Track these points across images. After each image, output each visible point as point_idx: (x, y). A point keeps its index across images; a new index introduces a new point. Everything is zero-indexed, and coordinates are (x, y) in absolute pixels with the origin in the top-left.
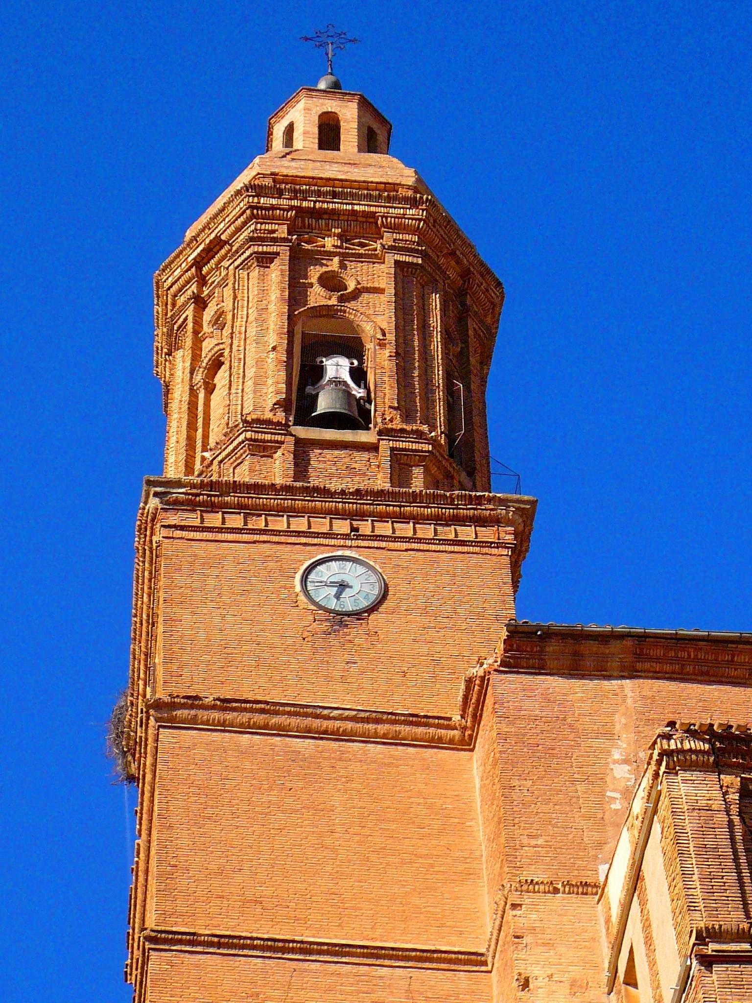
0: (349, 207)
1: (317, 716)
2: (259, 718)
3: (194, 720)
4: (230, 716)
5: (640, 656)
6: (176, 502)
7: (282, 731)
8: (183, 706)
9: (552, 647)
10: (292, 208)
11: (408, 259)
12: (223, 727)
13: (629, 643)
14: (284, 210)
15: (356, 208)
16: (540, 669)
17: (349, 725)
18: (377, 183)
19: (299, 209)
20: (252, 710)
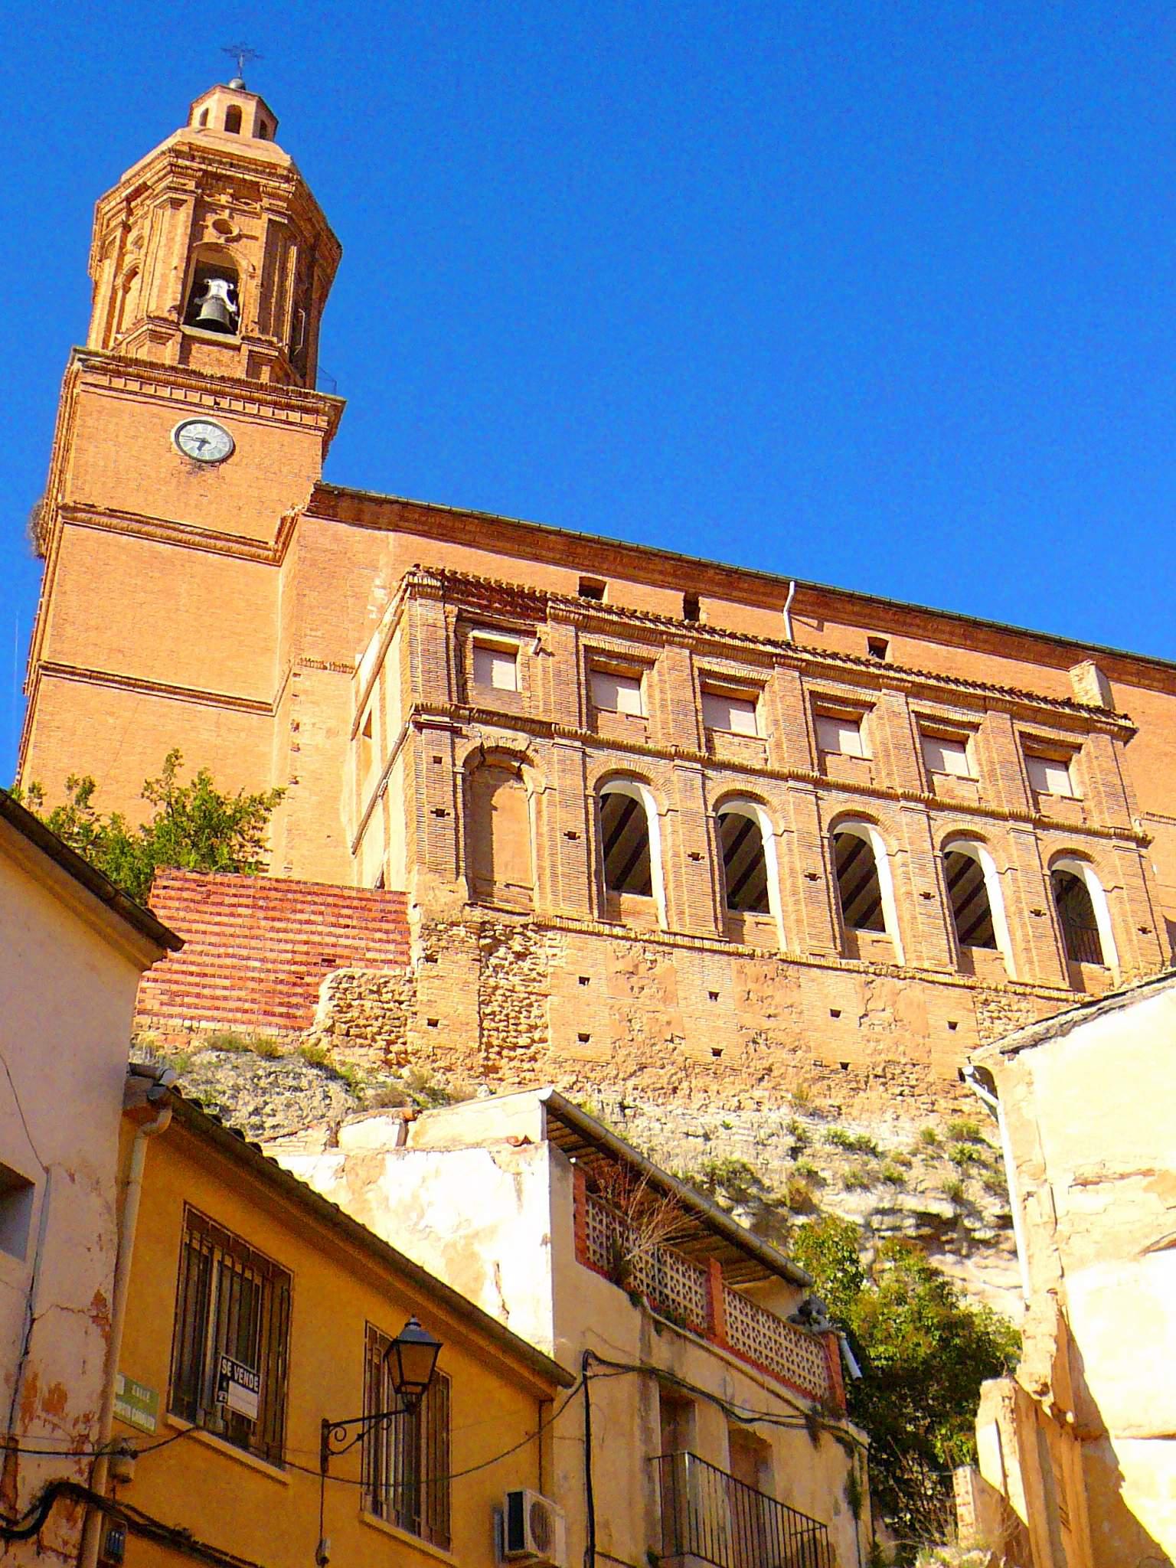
1: (175, 529)
2: (135, 526)
3: (90, 521)
4: (115, 521)
5: (402, 518)
6: (93, 367)
7: (149, 537)
8: (83, 511)
9: (345, 504)
10: (200, 170)
11: (278, 219)
12: (109, 529)
15: (247, 177)
16: (333, 517)
17: (198, 539)
19: (205, 172)
20: (131, 520)
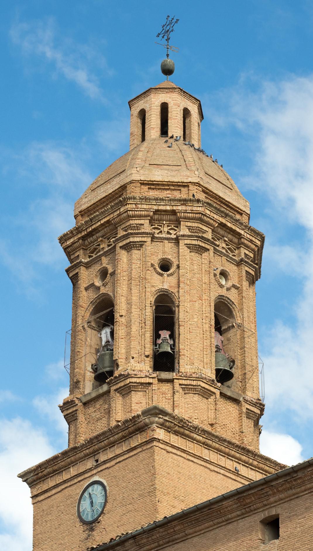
0: (99, 223)
10: (79, 239)
13: (131, 541)
14: (77, 242)
15: (102, 222)
18: (118, 189)
